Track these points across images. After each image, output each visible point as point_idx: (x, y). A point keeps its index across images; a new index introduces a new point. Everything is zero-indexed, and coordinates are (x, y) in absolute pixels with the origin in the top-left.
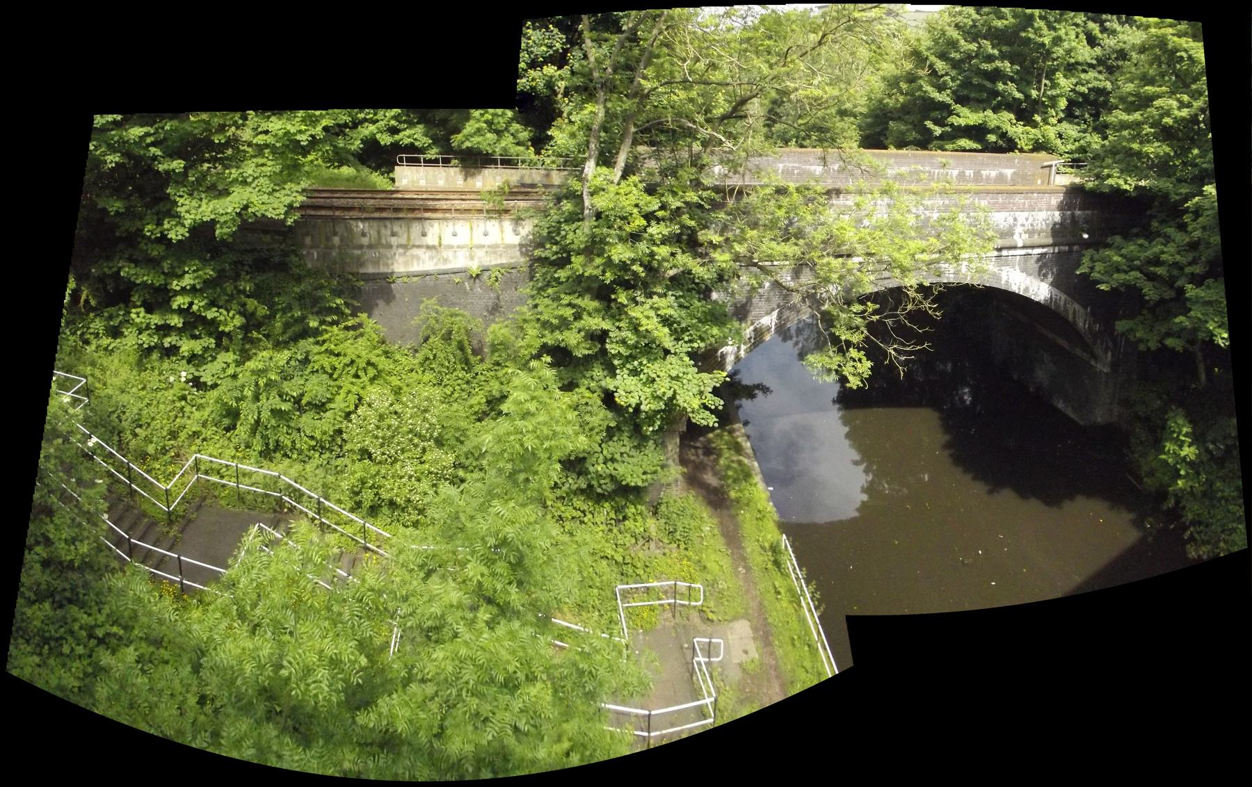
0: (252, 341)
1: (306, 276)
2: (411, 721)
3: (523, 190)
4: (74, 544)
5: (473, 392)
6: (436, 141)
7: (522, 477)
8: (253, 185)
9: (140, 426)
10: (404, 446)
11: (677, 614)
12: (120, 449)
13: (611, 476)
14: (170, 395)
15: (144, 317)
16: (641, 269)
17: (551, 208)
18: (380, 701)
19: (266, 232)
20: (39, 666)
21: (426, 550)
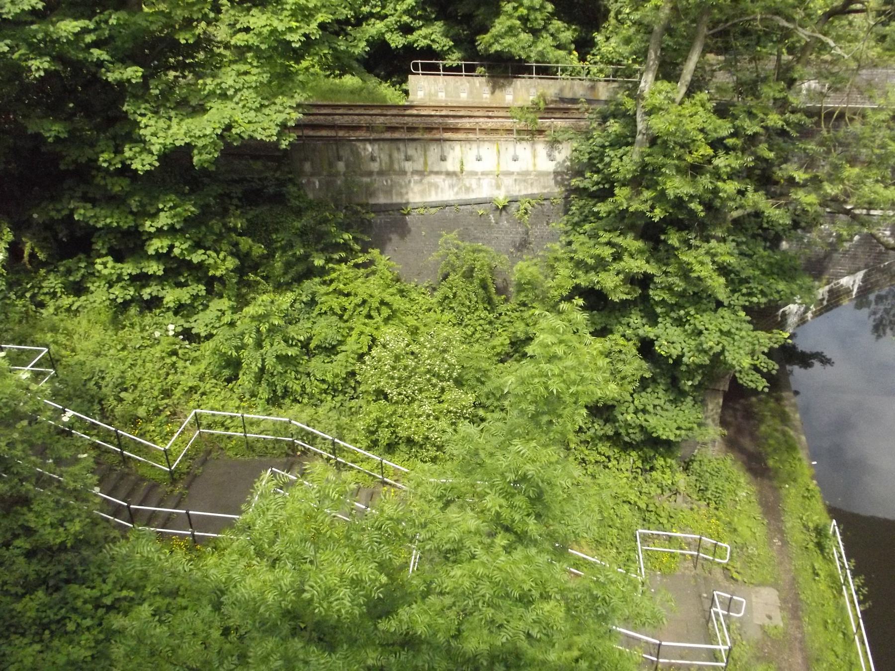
0: (249, 285)
1: (307, 208)
2: (429, 626)
3: (561, 106)
4: (62, 526)
5: (497, 333)
6: (458, 42)
7: (545, 419)
8: (236, 99)
9: (126, 390)
10: (422, 386)
11: (699, 566)
12: (104, 417)
13: (641, 426)
14: (157, 351)
15: (113, 268)
16: (700, 208)
17: (594, 129)
18: (400, 611)
19: (255, 158)
20: (41, 652)
21: (445, 483)
